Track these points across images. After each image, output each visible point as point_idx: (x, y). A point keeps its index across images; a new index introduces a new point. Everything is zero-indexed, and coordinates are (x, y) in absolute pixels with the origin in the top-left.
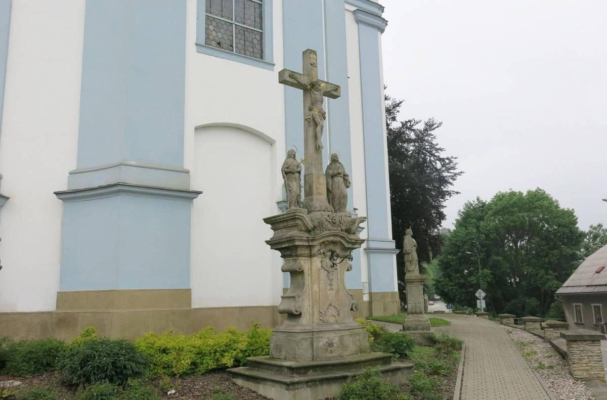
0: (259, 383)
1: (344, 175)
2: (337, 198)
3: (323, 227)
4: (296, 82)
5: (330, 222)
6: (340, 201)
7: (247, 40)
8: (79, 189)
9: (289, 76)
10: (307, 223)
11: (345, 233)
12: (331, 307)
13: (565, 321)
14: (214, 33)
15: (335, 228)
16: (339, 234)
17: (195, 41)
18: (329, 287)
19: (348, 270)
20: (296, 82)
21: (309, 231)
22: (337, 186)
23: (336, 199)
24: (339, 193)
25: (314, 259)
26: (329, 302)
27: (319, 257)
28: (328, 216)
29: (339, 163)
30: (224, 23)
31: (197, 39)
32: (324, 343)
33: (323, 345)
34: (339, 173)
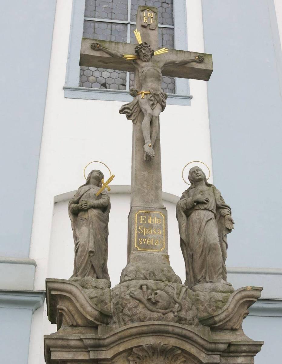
1: (218, 208)
2: (198, 255)
3: (125, 315)
4: (107, 56)
5: (140, 301)
6: (204, 260)
9: (92, 48)
10: (82, 306)
11: (196, 330)
13: (173, 25)
15: (156, 315)
16: (170, 329)
20: (107, 56)
21: (93, 326)
22: (196, 230)
23: (197, 256)
24: (202, 243)
28: (141, 288)
31: (66, 82)
34: (198, 203)
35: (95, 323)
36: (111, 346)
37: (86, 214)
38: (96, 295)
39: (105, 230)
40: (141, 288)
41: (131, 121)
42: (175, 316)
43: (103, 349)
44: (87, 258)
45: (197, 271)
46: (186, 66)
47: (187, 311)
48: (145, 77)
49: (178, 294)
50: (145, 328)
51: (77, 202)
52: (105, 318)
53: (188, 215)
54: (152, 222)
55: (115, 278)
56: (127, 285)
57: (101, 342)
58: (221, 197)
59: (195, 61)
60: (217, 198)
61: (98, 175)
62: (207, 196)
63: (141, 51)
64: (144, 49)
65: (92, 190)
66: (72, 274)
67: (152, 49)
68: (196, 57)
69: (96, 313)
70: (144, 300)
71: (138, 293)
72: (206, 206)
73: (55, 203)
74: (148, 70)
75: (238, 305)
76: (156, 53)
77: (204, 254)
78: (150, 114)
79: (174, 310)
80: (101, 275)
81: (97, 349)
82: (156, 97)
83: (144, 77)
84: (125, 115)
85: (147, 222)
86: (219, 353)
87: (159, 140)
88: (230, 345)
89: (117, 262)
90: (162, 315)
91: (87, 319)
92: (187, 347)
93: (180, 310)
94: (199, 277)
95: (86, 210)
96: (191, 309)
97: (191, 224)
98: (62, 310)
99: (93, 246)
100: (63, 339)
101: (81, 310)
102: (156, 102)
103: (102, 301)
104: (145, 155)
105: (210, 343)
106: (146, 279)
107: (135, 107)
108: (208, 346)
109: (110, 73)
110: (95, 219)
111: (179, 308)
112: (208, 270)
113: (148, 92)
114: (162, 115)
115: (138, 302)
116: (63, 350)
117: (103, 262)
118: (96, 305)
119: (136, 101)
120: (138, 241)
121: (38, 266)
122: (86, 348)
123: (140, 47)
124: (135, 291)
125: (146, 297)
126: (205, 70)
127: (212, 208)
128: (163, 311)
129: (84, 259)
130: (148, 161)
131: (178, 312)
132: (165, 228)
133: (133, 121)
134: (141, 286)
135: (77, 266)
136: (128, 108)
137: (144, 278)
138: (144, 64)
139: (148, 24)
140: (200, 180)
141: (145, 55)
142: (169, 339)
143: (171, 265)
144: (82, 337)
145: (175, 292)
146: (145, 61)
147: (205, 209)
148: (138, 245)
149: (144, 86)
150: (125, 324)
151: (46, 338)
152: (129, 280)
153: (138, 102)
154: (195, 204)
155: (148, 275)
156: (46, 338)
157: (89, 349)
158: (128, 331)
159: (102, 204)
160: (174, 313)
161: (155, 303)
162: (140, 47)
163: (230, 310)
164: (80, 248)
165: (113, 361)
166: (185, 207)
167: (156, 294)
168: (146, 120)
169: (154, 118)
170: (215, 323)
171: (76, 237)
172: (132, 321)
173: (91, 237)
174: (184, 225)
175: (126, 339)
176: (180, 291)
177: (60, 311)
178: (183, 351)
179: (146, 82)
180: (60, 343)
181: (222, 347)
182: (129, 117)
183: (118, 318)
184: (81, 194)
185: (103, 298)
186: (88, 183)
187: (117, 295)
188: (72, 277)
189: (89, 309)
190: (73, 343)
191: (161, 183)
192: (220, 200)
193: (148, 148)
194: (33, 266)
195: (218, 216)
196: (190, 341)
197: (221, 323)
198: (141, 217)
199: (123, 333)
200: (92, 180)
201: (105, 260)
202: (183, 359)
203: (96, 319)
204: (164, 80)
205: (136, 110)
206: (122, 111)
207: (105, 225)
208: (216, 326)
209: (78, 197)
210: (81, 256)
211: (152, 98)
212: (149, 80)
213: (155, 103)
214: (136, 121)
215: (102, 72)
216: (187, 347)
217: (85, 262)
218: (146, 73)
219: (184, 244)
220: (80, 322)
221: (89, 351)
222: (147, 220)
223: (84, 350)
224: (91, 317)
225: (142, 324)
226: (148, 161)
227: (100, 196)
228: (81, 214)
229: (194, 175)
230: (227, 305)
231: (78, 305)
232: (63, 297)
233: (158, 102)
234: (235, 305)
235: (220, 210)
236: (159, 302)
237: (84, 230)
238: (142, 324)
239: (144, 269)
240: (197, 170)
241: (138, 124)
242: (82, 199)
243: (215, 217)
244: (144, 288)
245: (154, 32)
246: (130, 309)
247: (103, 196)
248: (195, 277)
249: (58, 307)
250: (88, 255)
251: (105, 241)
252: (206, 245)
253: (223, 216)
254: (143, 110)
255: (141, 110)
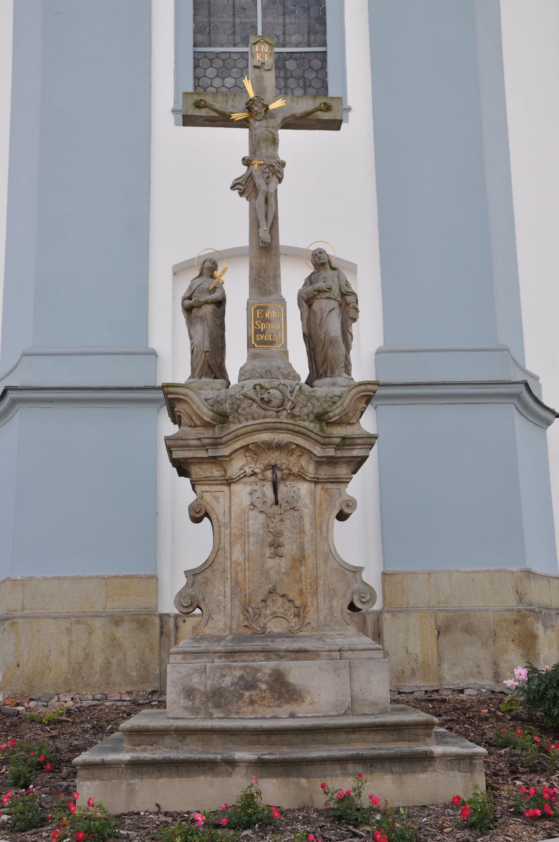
0: (325, 764)
3: (239, 414)
4: (216, 114)
5: (254, 400)
7: (292, 77)
8: (27, 385)
12: (274, 597)
14: (217, 82)
17: (171, 105)
18: (268, 552)
19: (342, 516)
20: (216, 114)
25: (235, 488)
26: (271, 586)
27: (245, 483)
29: (333, 269)
30: (239, 56)
32: (236, 680)
33: (232, 684)
34: (319, 291)
35: (212, 424)
36: (228, 444)
37: (200, 310)
38: (212, 396)
39: (222, 326)
40: (254, 388)
41: (244, 198)
42: (288, 414)
43: (220, 447)
44: (203, 358)
45: (319, 365)
46: (309, 117)
47: (301, 408)
48: (259, 142)
49: (292, 392)
50: (258, 426)
51: (190, 298)
52: (223, 418)
53: (310, 306)
54: (270, 316)
55: (233, 377)
56: (242, 385)
57: (219, 441)
58: (347, 281)
59: (321, 110)
60: (341, 284)
61: (211, 265)
62: (329, 283)
63: (253, 108)
64: (256, 106)
65: (205, 283)
66: (189, 374)
67: (265, 103)
68: (321, 105)
69: (211, 413)
70: (258, 400)
71: (251, 393)
72: (327, 295)
73: (175, 274)
74: (262, 133)
75: (354, 399)
76: (271, 107)
77: (325, 347)
78: (264, 191)
79: (287, 408)
80: (219, 375)
81: (215, 447)
82: (271, 168)
83: (257, 142)
84: (237, 191)
85: (265, 316)
86: (333, 447)
87: (277, 219)
88: (344, 438)
89: (236, 358)
90: (275, 413)
91: (204, 420)
92: (300, 441)
93: (294, 408)
94: (321, 372)
95: (199, 307)
96: (306, 406)
97: (312, 314)
98: (179, 412)
99: (209, 346)
100: (182, 439)
101: (198, 411)
102: (272, 174)
103: (218, 402)
104: (260, 240)
105: (324, 437)
106: (262, 378)
107: (248, 181)
108: (322, 440)
109: (236, 79)
110: (209, 317)
111: (293, 405)
112: (329, 365)
113: (262, 162)
114: (280, 186)
115: (252, 401)
116: (183, 449)
117: (220, 360)
118: (212, 406)
119: (249, 173)
120: (255, 337)
121: (159, 355)
122: (204, 447)
123: (251, 102)
124: (248, 391)
125: (259, 397)
126: (334, 121)
127: (336, 296)
128: (276, 409)
129: (200, 359)
130: (265, 249)
131: (291, 409)
132: (284, 322)
133: (247, 198)
134: (255, 385)
135: (194, 367)
136: (240, 184)
137: (260, 377)
138: (257, 123)
139: (262, 63)
140: (323, 264)
141: (258, 113)
142: (283, 435)
143: (290, 361)
144: (199, 437)
145: (288, 390)
146: (258, 120)
147: (328, 298)
148: (255, 341)
149: (258, 153)
150: (240, 423)
151: (167, 439)
152: (245, 380)
153: (251, 173)
154: (316, 293)
155: (264, 374)
156: (167, 439)
157: (208, 447)
158: (243, 429)
159: (216, 300)
160: (287, 411)
161: (269, 402)
162: (251, 102)
163: (345, 405)
164: (195, 348)
165: (232, 457)
166: (305, 297)
167: (269, 393)
168: (261, 199)
169: (269, 195)
170: (330, 418)
171: (191, 338)
172: (247, 420)
173: (207, 336)
174: (306, 316)
175: (242, 437)
176: (294, 389)
177: (178, 414)
178: (298, 446)
179: (260, 148)
180: (180, 442)
181: (337, 441)
182: (241, 194)
183: (234, 417)
184: (193, 288)
185: (219, 399)
186: (201, 275)
187: (232, 396)
188: (189, 378)
189: (205, 410)
190: (192, 443)
191: (280, 271)
192: (345, 286)
193: (264, 228)
194: (154, 357)
195: (344, 304)
196: (304, 437)
197: (336, 418)
198: (258, 311)
199: (237, 432)
200: (204, 271)
201: (223, 359)
202: (299, 454)
203: (212, 420)
204: (312, 84)
205: (249, 185)
206: (233, 188)
207: (220, 321)
208: (331, 421)
209: (191, 293)
210: (197, 356)
211: (267, 170)
212: (263, 145)
213: (270, 176)
214: (250, 198)
215: (224, 79)
216: (300, 441)
217: (202, 362)
218: (259, 137)
219: (308, 338)
220: (198, 422)
221: (207, 450)
222: (264, 313)
223: (203, 448)
224: (208, 417)
225: (256, 422)
226: (265, 249)
227: (215, 289)
228: (194, 310)
229: (317, 259)
230: (342, 400)
231: (194, 407)
232: (180, 400)
233: (273, 174)
234: (351, 399)
235: (346, 297)
236: (272, 401)
237: (199, 329)
238: (256, 422)
239: (260, 367)
240: (320, 253)
241: (253, 200)
242: (194, 294)
243: (340, 305)
244: (258, 388)
245: (269, 72)
246: (244, 409)
247: (217, 291)
248: (317, 372)
249: (176, 409)
250: (204, 355)
251: (221, 338)
252: (327, 338)
253: (347, 304)
254: (257, 186)
255: (255, 185)
